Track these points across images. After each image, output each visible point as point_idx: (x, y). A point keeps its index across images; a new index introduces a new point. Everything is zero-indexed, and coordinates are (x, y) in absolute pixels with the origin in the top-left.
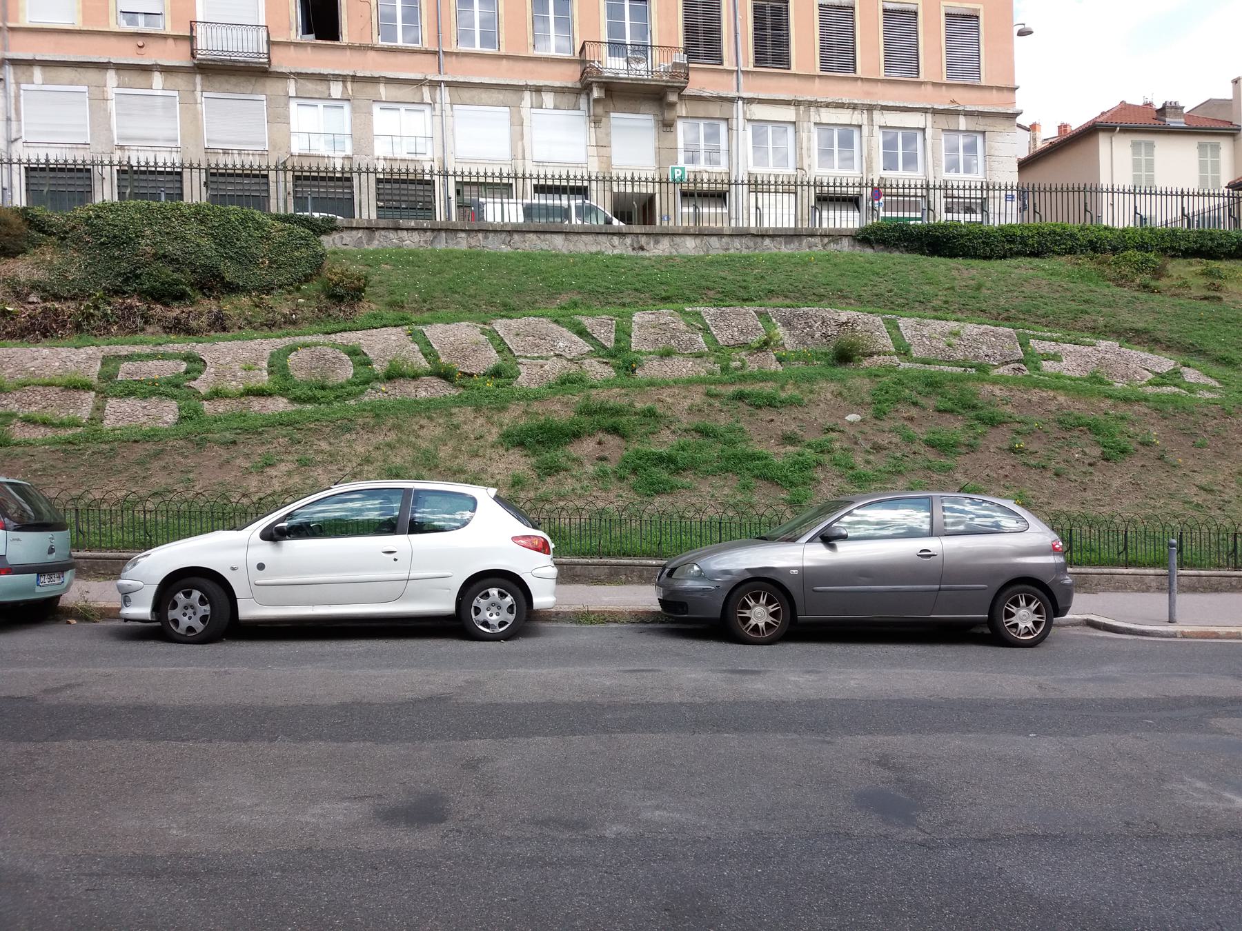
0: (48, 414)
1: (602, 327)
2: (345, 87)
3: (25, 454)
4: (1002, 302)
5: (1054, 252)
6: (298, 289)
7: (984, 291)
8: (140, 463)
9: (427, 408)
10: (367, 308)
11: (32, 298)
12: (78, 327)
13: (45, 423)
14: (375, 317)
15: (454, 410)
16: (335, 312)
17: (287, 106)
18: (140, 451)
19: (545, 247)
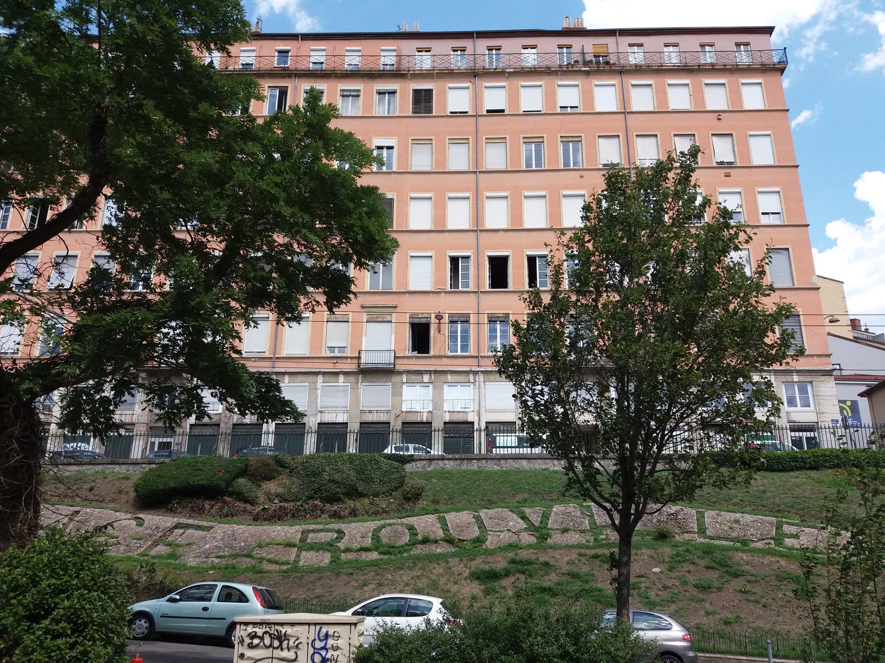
0: (277, 558)
1: (534, 514)
2: (431, 376)
3: (268, 577)
4: (778, 500)
5: (825, 466)
6: (391, 495)
7: (768, 494)
8: (313, 583)
9: (438, 558)
10: (423, 503)
11: (276, 501)
12: (293, 516)
13: (276, 563)
14: (423, 509)
15: (450, 560)
16: (406, 506)
17: (402, 387)
18: (313, 577)
19: (518, 466)
